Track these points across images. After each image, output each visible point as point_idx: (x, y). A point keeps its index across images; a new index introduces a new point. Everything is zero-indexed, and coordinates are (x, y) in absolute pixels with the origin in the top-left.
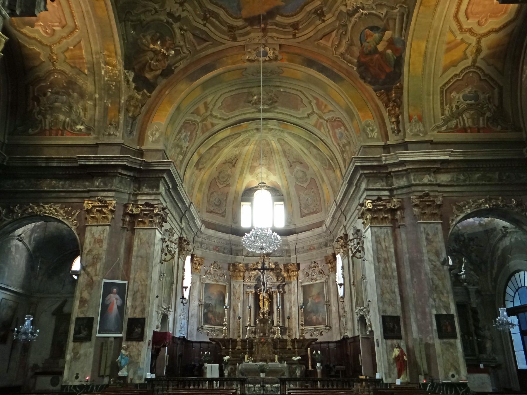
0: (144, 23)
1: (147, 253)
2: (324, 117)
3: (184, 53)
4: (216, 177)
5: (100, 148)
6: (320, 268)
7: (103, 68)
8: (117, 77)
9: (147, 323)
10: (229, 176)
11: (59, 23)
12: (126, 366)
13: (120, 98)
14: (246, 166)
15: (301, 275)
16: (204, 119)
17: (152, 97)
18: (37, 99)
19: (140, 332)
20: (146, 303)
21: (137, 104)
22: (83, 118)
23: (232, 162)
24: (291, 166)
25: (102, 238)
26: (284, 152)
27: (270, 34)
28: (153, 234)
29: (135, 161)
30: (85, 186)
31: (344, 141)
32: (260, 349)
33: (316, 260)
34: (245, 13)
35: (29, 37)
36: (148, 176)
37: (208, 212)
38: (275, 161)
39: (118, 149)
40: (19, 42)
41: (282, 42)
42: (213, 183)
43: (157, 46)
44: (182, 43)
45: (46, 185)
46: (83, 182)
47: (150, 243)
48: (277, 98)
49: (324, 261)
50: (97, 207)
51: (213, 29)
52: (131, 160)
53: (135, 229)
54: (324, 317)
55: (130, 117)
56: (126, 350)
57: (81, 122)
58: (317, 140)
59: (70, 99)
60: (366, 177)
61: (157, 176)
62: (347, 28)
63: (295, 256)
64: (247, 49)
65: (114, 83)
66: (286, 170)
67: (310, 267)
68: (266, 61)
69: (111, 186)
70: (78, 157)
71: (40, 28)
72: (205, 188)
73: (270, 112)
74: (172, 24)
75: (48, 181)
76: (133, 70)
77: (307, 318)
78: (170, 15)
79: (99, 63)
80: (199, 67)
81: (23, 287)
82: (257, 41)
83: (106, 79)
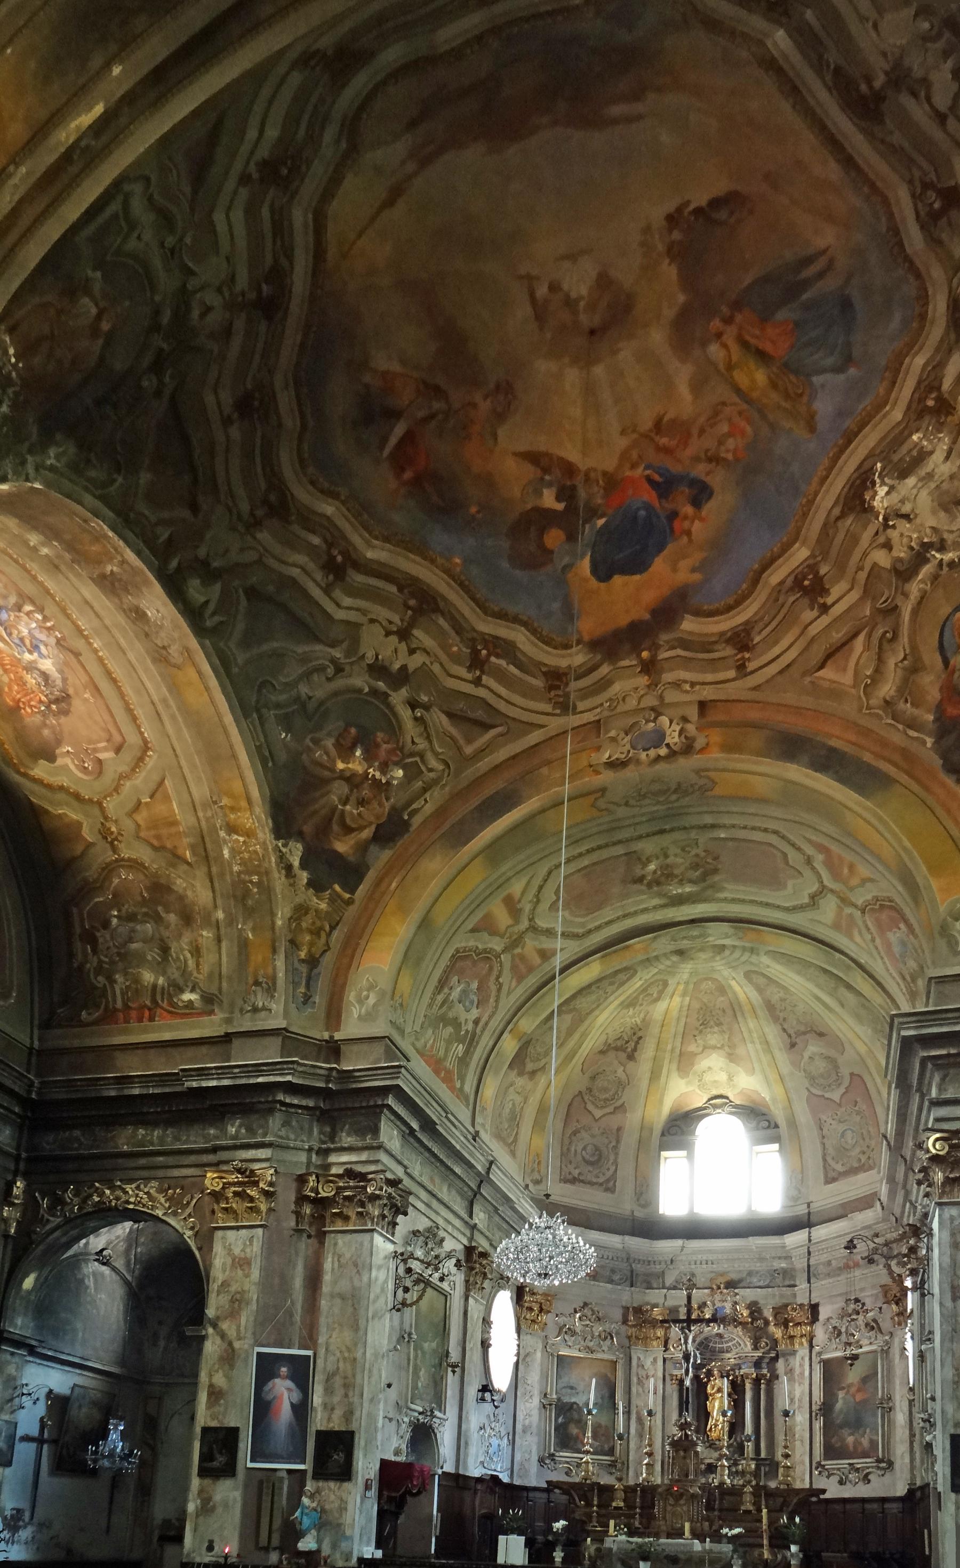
0: (311, 706)
1: (354, 1288)
2: (853, 900)
3: (430, 770)
4: (583, 1089)
5: (236, 1043)
6: (870, 1314)
7: (225, 841)
8: (259, 860)
9: (360, 1442)
10: (622, 1085)
11: (108, 741)
12: (314, 1532)
13: (273, 914)
14: (667, 1055)
15: (820, 1333)
16: (517, 942)
17: (357, 903)
18: (90, 938)
19: (342, 1460)
20: (356, 1400)
21: (318, 924)
22: (195, 974)
23: (627, 1046)
24: (793, 1045)
25: (248, 1256)
26: (770, 1007)
27: (668, 677)
28: (366, 1244)
29: (312, 1070)
30: (207, 1138)
31: (912, 964)
32: (669, 1508)
33: (860, 1295)
34: (588, 626)
35: (49, 787)
36: (350, 1105)
37: (566, 1181)
38: (746, 1035)
39: (275, 1043)
40: (31, 803)
41: (707, 693)
42: (576, 1105)
43: (356, 764)
44: (422, 744)
45: (126, 1139)
46: (204, 1129)
47: (360, 1265)
48: (716, 858)
49: (881, 1296)
50: (234, 1184)
51: (502, 691)
52: (301, 1069)
53: (325, 1233)
54: (875, 1438)
55: (303, 961)
56: (312, 1497)
57: (190, 985)
58: (849, 967)
59: (162, 929)
60: (937, 1067)
61: (372, 1103)
62: (899, 615)
63: (805, 1285)
64: (607, 732)
65: (255, 878)
66: (782, 1057)
67: (843, 1314)
68: (658, 758)
69: (265, 1135)
70: (183, 1070)
71: (68, 761)
72: (553, 1122)
73: (705, 900)
74: (386, 695)
75: (130, 1129)
76: (300, 836)
77: (833, 1440)
78: (378, 669)
79: (214, 830)
80: (475, 802)
81: (122, 1362)
82: (632, 703)
83: (236, 868)
